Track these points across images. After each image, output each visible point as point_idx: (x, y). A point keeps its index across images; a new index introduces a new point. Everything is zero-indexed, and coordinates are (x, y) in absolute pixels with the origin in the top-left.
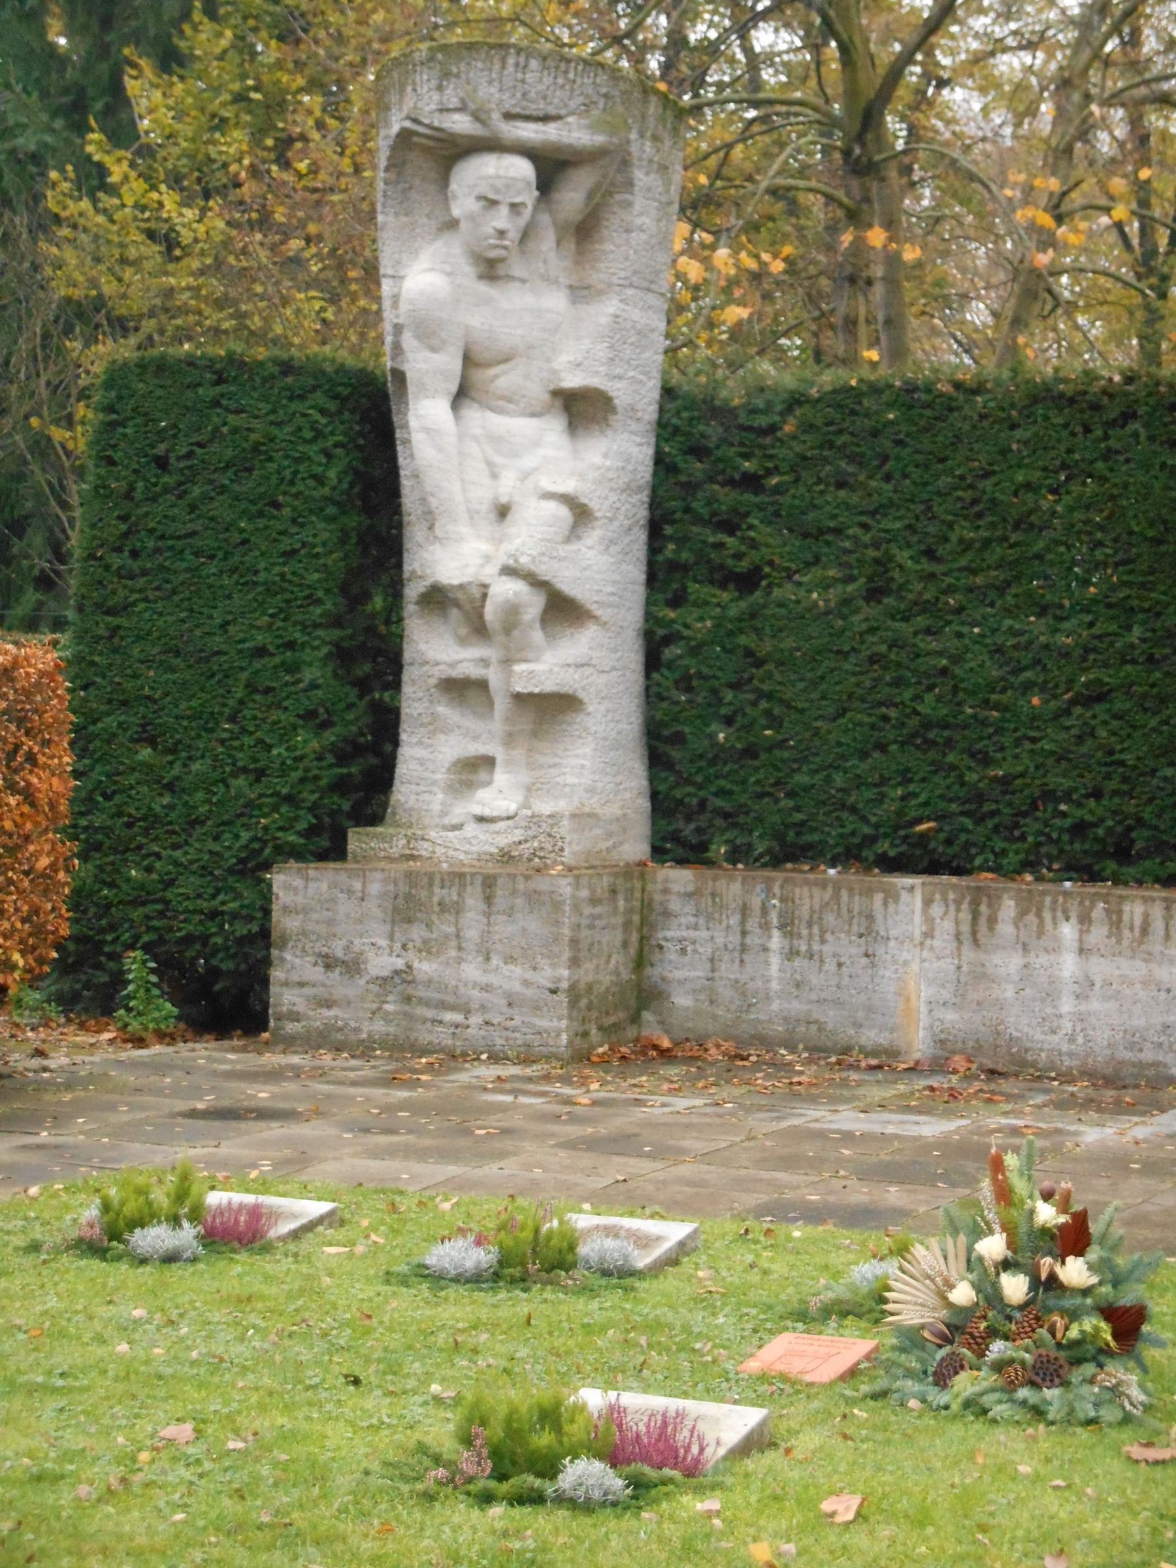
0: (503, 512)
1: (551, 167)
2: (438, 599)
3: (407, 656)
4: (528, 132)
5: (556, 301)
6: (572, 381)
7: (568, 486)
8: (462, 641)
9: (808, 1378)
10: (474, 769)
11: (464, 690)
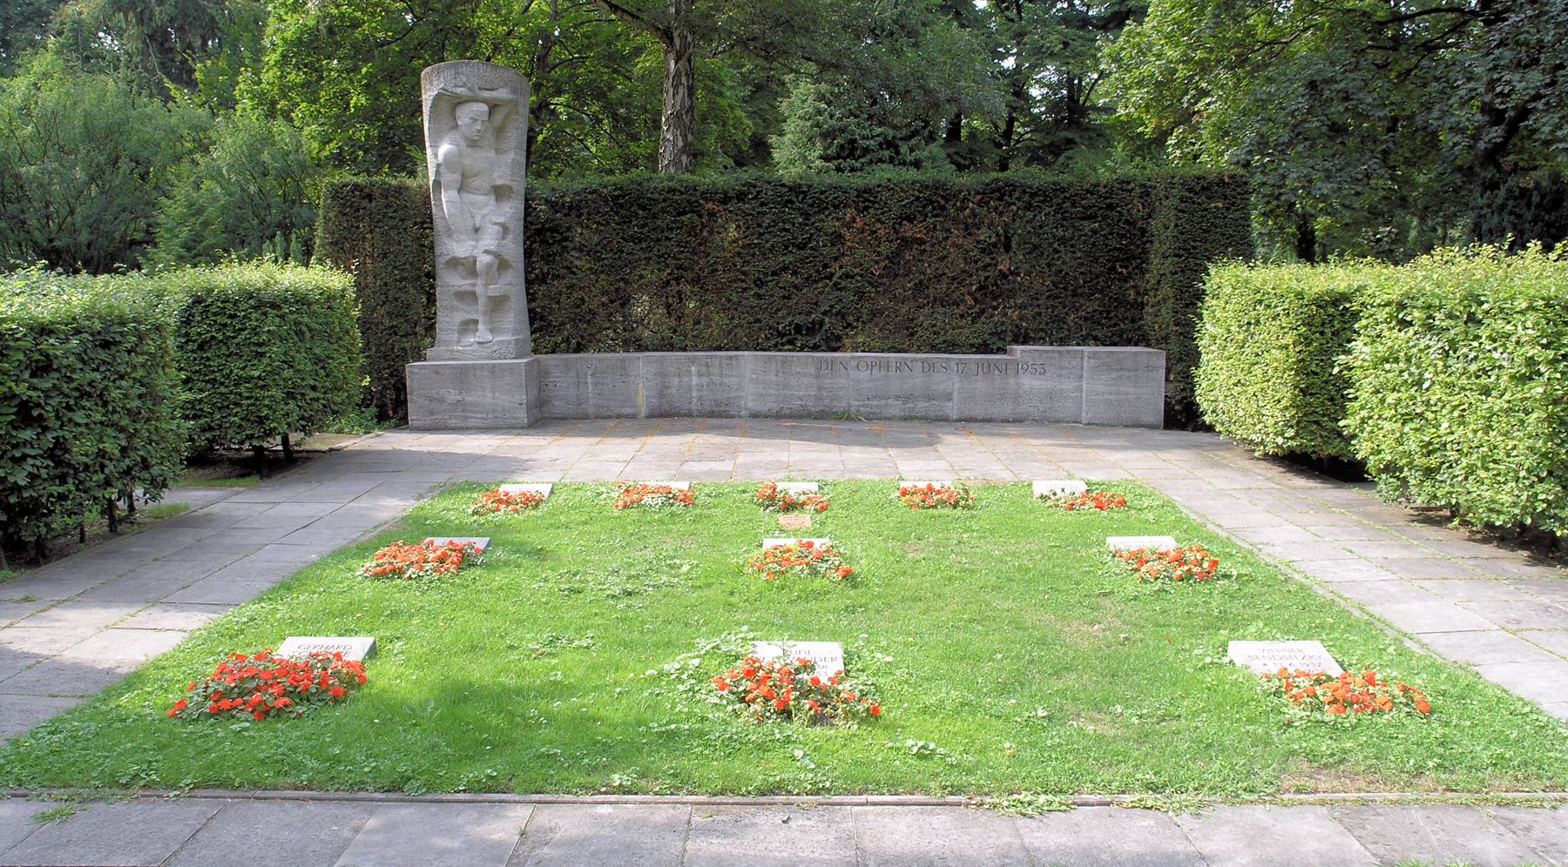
0: (477, 230)
1: (493, 107)
2: (454, 263)
3: (590, 357)
4: (486, 94)
5: (492, 154)
6: (499, 182)
7: (502, 220)
8: (464, 278)
9: (13, 647)
10: (469, 326)
11: (468, 297)
